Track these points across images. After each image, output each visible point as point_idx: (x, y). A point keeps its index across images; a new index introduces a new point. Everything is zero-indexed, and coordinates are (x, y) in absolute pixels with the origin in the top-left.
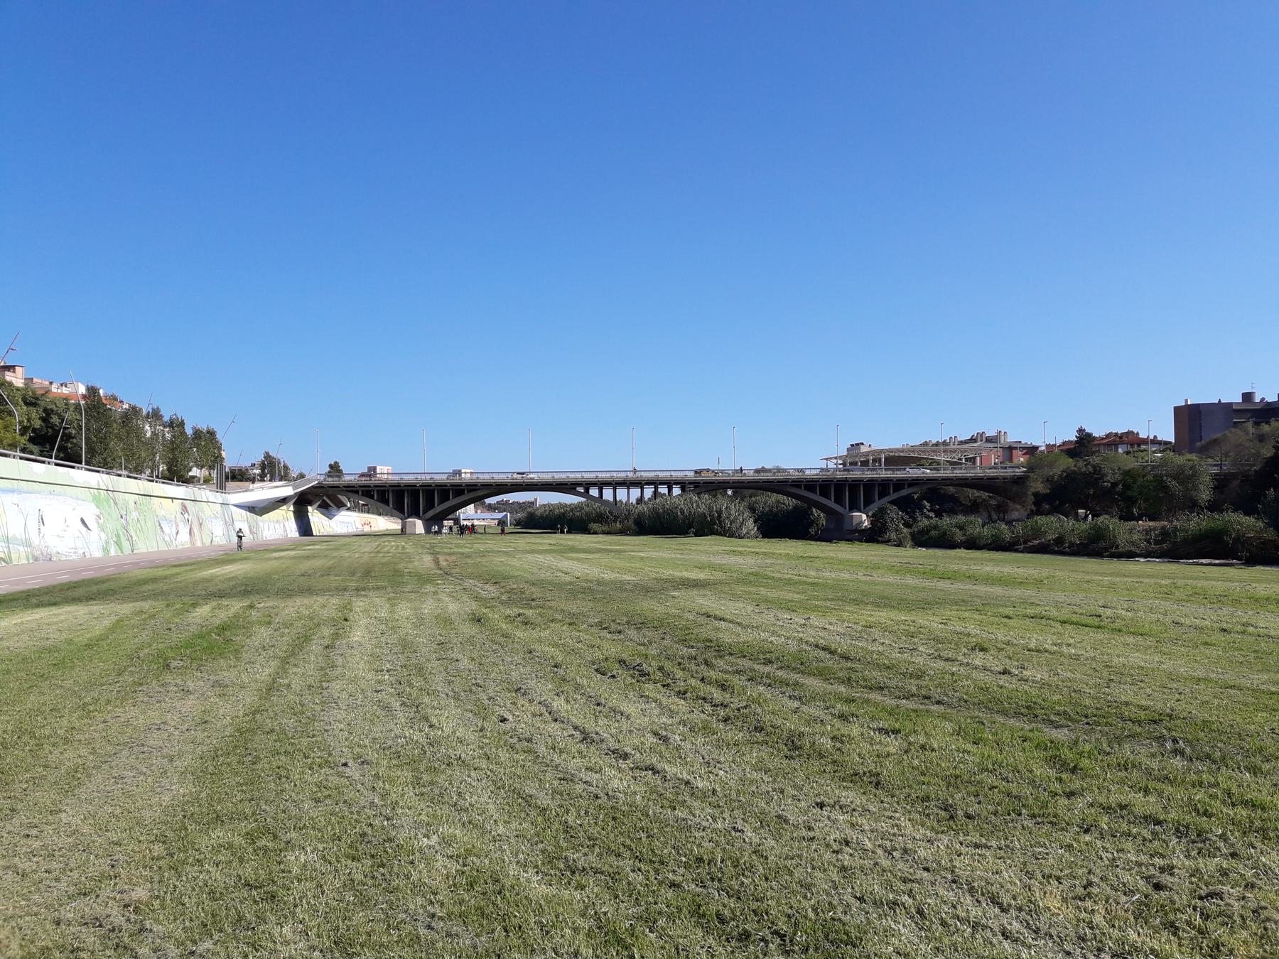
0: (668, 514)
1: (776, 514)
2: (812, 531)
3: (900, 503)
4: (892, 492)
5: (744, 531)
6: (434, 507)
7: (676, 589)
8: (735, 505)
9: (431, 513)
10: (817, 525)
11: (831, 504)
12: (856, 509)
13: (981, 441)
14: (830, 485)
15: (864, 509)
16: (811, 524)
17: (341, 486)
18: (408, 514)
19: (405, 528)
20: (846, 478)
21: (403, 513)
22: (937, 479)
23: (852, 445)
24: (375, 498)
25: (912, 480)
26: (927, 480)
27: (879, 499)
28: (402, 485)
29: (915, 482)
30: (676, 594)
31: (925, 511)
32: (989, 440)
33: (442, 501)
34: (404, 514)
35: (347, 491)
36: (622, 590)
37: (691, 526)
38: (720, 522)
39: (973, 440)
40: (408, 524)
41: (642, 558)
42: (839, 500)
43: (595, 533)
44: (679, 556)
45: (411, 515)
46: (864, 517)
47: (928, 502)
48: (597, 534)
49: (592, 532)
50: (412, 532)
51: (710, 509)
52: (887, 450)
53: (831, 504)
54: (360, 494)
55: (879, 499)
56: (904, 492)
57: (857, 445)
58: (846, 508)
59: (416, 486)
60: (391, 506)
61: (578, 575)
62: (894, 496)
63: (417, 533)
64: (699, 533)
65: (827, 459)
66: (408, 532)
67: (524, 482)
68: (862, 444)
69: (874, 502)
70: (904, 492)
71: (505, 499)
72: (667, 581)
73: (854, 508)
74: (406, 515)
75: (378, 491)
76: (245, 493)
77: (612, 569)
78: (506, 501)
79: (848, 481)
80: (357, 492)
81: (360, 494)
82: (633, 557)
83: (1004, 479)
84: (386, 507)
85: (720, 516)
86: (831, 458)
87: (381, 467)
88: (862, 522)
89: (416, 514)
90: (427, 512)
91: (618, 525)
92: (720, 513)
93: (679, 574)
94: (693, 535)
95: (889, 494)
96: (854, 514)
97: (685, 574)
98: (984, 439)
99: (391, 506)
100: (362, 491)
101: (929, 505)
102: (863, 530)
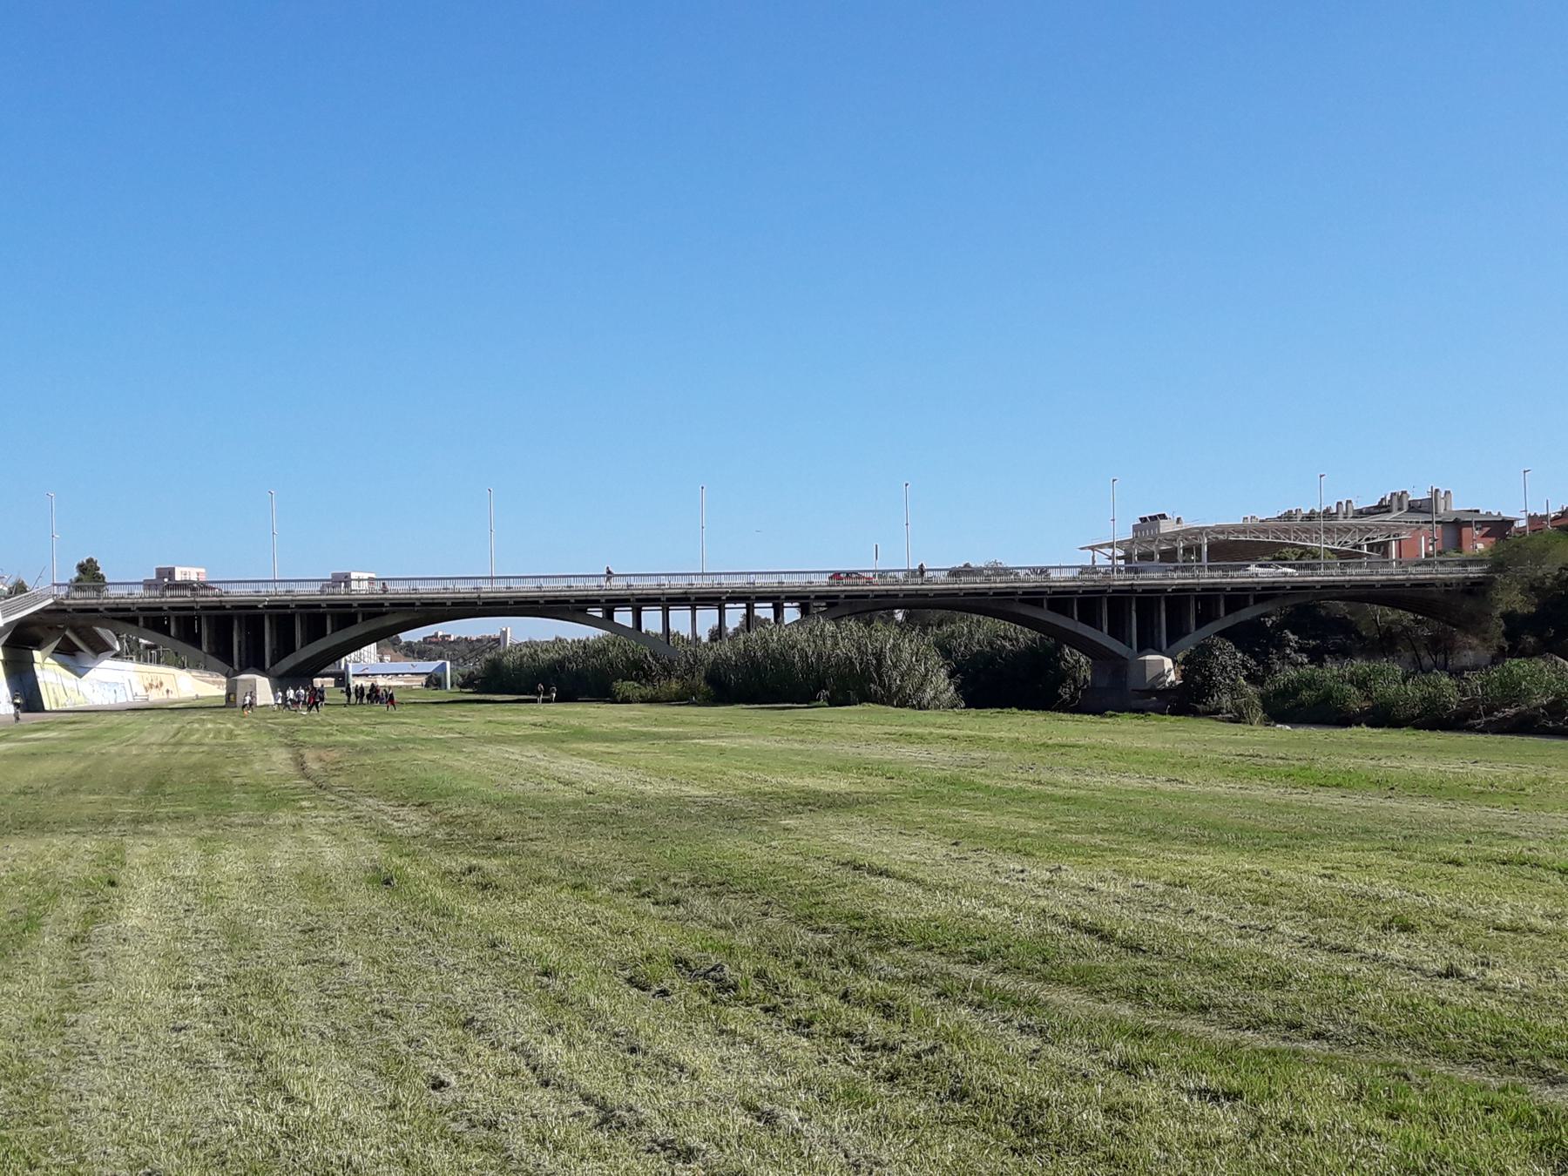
4: (1222, 613)
11: (1103, 638)
12: (1154, 648)
13: (1400, 509)
15: (1168, 646)
16: (1061, 677)
23: (1143, 520)
30: (790, 822)
32: (1414, 508)
34: (232, 666)
35: (114, 618)
36: (682, 816)
37: (821, 685)
38: (880, 676)
39: (1383, 508)
40: (239, 685)
41: (722, 752)
42: (1118, 631)
43: (626, 701)
45: (248, 667)
47: (1294, 634)
48: (630, 702)
49: (619, 698)
52: (1213, 530)
53: (1103, 638)
54: (141, 623)
56: (1247, 614)
57: (1153, 518)
58: (1131, 647)
60: (205, 648)
62: (1228, 621)
65: (1092, 548)
67: (479, 598)
68: (1163, 517)
70: (1247, 614)
71: (440, 634)
72: (774, 796)
74: (236, 667)
77: (661, 774)
78: (443, 637)
81: (141, 623)
82: (704, 749)
83: (1446, 585)
86: (1101, 546)
88: (1162, 674)
91: (675, 686)
92: (879, 656)
93: (797, 782)
95: (1217, 617)
96: (1148, 657)
97: (811, 783)
98: (1406, 508)
99: (205, 648)
101: (1296, 638)
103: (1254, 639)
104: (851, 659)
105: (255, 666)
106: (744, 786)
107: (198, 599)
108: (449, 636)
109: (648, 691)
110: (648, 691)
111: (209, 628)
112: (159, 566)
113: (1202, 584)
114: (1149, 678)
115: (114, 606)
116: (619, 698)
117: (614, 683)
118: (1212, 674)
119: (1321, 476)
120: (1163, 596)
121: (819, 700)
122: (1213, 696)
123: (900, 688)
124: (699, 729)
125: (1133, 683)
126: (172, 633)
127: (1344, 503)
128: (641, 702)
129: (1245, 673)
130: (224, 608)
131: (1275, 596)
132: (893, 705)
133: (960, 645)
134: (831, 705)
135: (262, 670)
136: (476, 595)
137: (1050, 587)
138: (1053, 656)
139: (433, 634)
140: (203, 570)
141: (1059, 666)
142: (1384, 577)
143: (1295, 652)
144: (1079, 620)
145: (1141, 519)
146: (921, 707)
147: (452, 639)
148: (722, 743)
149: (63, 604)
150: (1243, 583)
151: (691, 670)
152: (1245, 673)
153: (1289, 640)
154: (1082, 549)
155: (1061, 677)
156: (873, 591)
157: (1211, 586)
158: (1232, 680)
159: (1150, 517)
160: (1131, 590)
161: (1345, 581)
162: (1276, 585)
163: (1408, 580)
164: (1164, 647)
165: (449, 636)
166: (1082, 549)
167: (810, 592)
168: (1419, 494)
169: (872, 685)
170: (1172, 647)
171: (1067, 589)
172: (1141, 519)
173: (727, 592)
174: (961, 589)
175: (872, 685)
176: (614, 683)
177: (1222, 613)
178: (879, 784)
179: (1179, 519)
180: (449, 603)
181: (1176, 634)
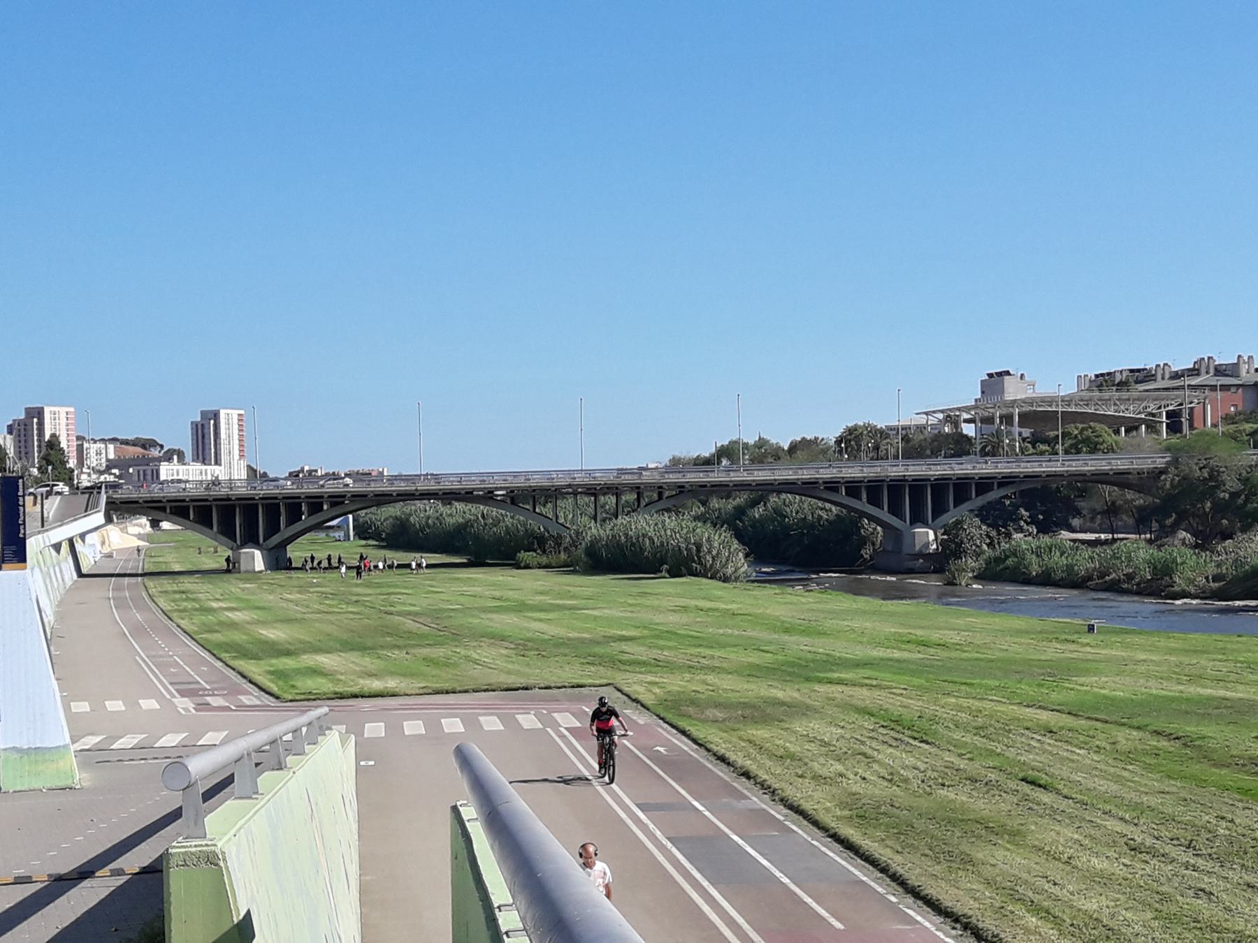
0: (633, 544)
1: (812, 526)
2: (866, 553)
3: (984, 514)
4: (974, 496)
5: (730, 570)
6: (278, 530)
7: (614, 642)
8: (720, 535)
9: (276, 539)
10: (873, 544)
11: (884, 515)
12: (923, 523)
13: (1207, 373)
14: (881, 487)
15: (933, 521)
16: (863, 541)
17: (141, 501)
18: (241, 542)
19: (239, 563)
20: (904, 476)
21: (232, 536)
22: (1040, 476)
23: (990, 375)
24: (192, 517)
25: (1003, 478)
26: (1025, 477)
27: (955, 507)
28: (233, 498)
29: (1006, 481)
30: (612, 644)
31: (1022, 523)
32: (1220, 371)
33: (290, 522)
34: (235, 542)
35: (148, 507)
36: (583, 643)
37: (663, 562)
38: (699, 558)
39: (1194, 372)
40: (242, 556)
41: (596, 618)
42: (896, 510)
43: (527, 567)
44: (629, 615)
45: (246, 543)
46: (931, 533)
47: (1026, 511)
48: (530, 568)
49: (522, 565)
50: (250, 568)
51: (687, 540)
52: (1024, 401)
53: (884, 515)
54: (168, 511)
55: (955, 507)
56: (993, 495)
57: (1000, 374)
58: (905, 522)
59: (254, 499)
60: (215, 528)
61: (553, 634)
62: (979, 501)
63: (256, 570)
64: (675, 573)
65: (927, 413)
66: (242, 568)
67: (417, 490)
68: (1008, 373)
69: (948, 511)
70: (993, 495)
71: (306, 468)
72: (611, 637)
73: (918, 519)
74: (238, 542)
75: (194, 506)
76: (62, 528)
77: (574, 630)
78: (310, 472)
79: (907, 480)
80: (163, 509)
81: (168, 511)
82: (588, 616)
83: (1138, 473)
84: (210, 531)
85: (698, 551)
86: (934, 412)
87: (53, 409)
88: (927, 545)
89: (251, 539)
90: (268, 539)
91: (563, 556)
92: (699, 547)
93: (619, 633)
94: (667, 576)
95: (969, 499)
96: (917, 530)
97: (624, 633)
98: (1212, 371)
99: (215, 528)
100: (171, 508)
101: (1028, 514)
102: (929, 554)
103: (998, 518)
104: (679, 547)
105: (252, 542)
106: (603, 634)
107: (211, 493)
108: (316, 471)
109: (544, 560)
110: (544, 560)
111: (218, 515)
112: (28, 406)
113: (957, 474)
114: (917, 548)
115: (150, 499)
116: (522, 565)
117: (518, 554)
118: (962, 542)
119: (1059, 385)
120: (929, 483)
121: (662, 572)
122: (962, 559)
123: (712, 566)
124: (583, 601)
125: (906, 549)
126: (191, 518)
127: (1162, 366)
128: (539, 568)
129: (988, 541)
130: (230, 500)
131: (1014, 482)
132: (708, 578)
133: (791, 511)
134: (672, 576)
135: (256, 544)
136: (414, 488)
137: (843, 478)
138: (855, 525)
139: (299, 469)
140: (72, 409)
141: (860, 533)
142: (1093, 468)
143: (1028, 524)
144: (868, 503)
145: (988, 375)
146: (726, 579)
147: (319, 474)
148: (596, 613)
149: (112, 498)
150: (988, 473)
151: (574, 544)
152: (988, 541)
153: (1022, 516)
154: (917, 414)
155: (863, 541)
156: (710, 482)
157: (964, 476)
158: (978, 546)
159: (996, 373)
160: (903, 479)
161: (1063, 471)
162: (1013, 475)
163: (1111, 470)
164: (930, 522)
165: (316, 471)
166: (917, 414)
167: (663, 483)
168: (1225, 358)
169: (693, 564)
170: (935, 522)
171: (856, 479)
172: (988, 375)
173: (600, 484)
174: (775, 480)
175: (693, 564)
176: (518, 554)
177: (974, 496)
178: (646, 632)
179: (1022, 375)
180: (394, 494)
181: (939, 510)
